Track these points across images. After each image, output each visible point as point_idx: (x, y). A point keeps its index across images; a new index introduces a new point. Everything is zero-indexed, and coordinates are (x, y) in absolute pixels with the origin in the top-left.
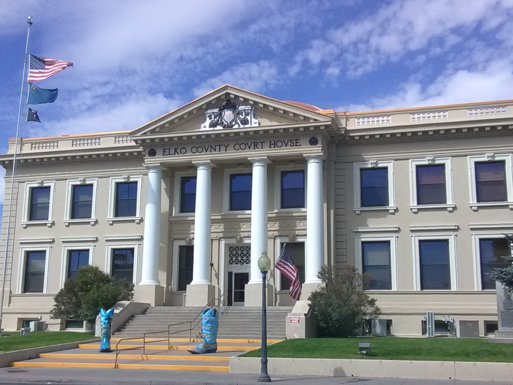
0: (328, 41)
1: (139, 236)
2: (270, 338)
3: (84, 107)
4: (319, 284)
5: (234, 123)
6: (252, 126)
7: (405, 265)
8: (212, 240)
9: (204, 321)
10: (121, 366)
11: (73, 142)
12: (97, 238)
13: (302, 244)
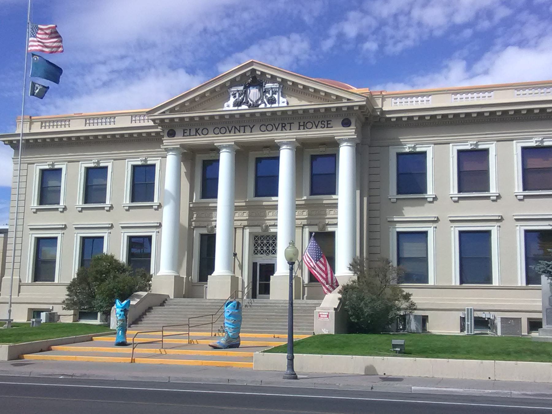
0: (365, 12)
1: (63, 225)
2: (297, 333)
3: (99, 83)
4: (350, 277)
5: (260, 102)
6: (280, 105)
7: (443, 257)
8: (235, 228)
9: (227, 314)
10: (138, 360)
11: (132, 118)
12: (112, 225)
13: (333, 234)
